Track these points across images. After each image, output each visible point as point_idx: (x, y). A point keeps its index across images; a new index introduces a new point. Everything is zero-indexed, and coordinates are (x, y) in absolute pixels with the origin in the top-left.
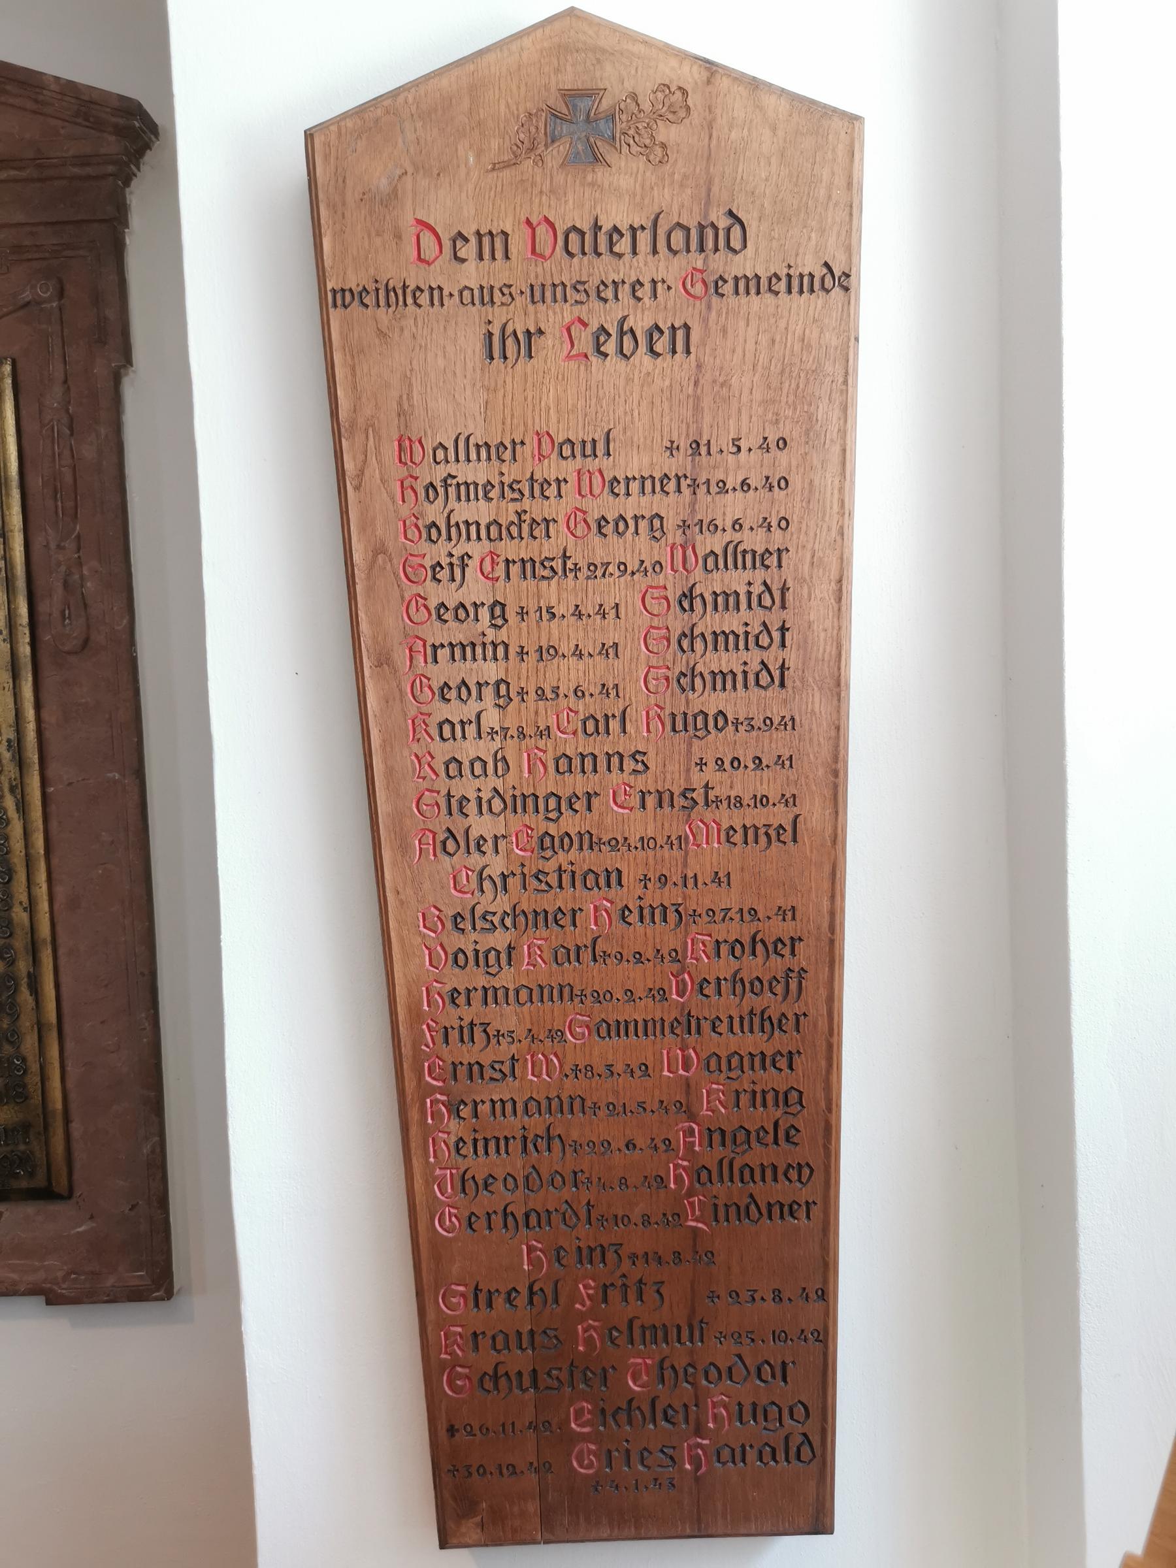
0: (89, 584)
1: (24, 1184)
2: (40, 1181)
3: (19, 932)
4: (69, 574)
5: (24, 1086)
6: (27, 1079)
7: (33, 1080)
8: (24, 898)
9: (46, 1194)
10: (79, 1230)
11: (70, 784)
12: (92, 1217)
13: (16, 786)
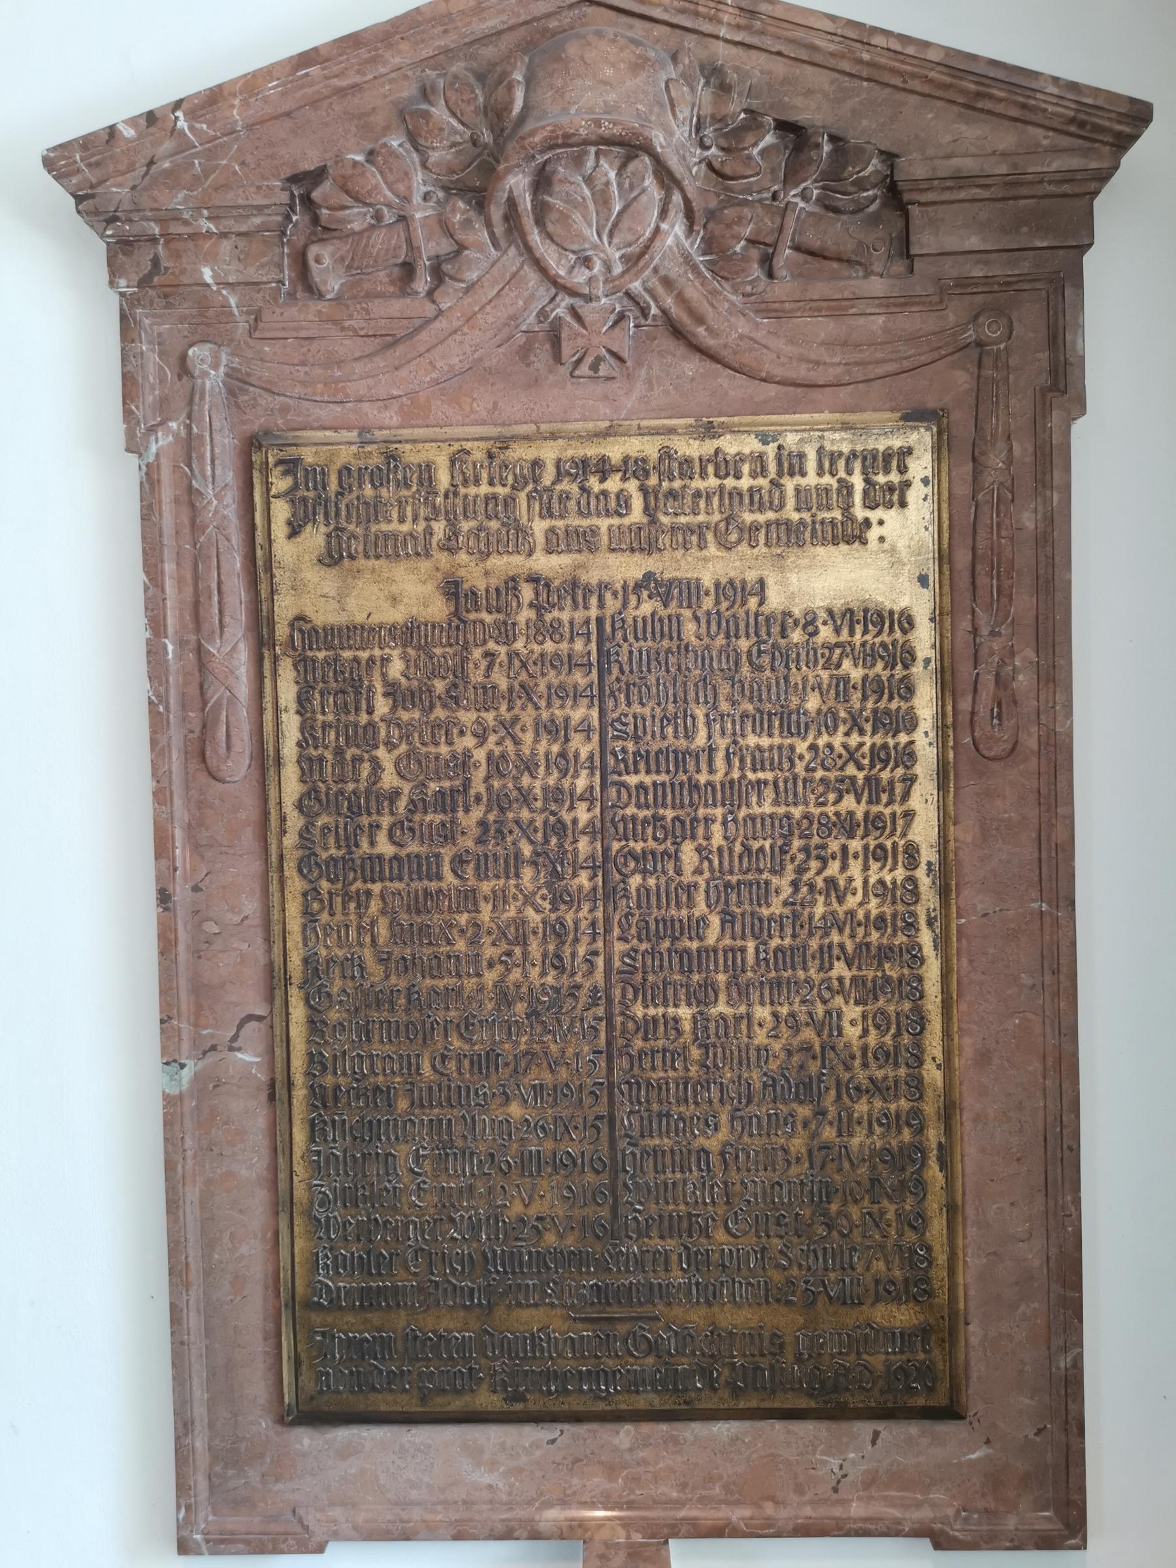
0: (1021, 677)
1: (921, 1402)
2: (941, 1399)
3: (930, 1094)
4: (1002, 663)
5: (927, 1281)
6: (933, 1272)
7: (939, 1274)
8: (938, 1052)
9: (951, 1412)
10: (973, 1456)
11: (985, 915)
12: (988, 1442)
13: (935, 918)
